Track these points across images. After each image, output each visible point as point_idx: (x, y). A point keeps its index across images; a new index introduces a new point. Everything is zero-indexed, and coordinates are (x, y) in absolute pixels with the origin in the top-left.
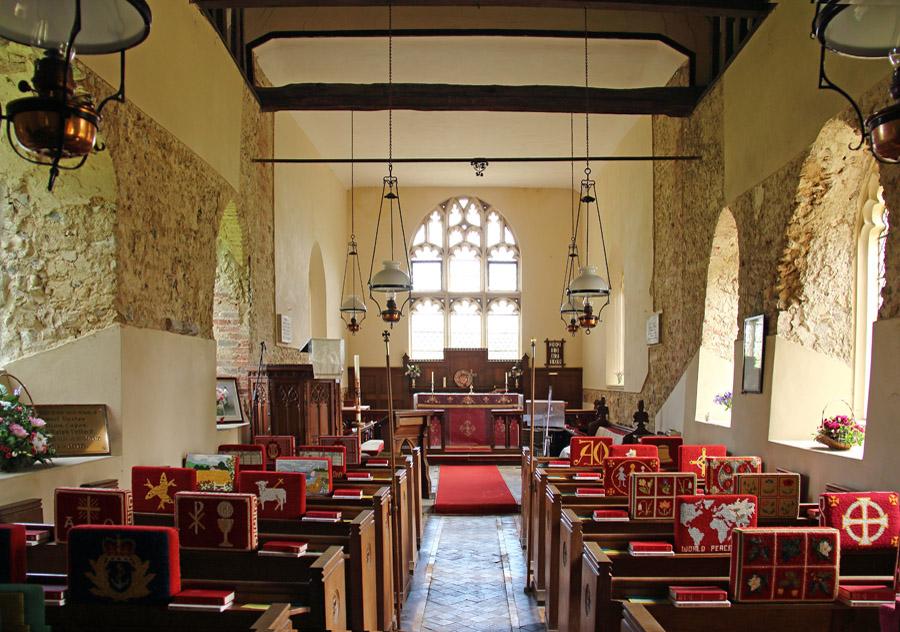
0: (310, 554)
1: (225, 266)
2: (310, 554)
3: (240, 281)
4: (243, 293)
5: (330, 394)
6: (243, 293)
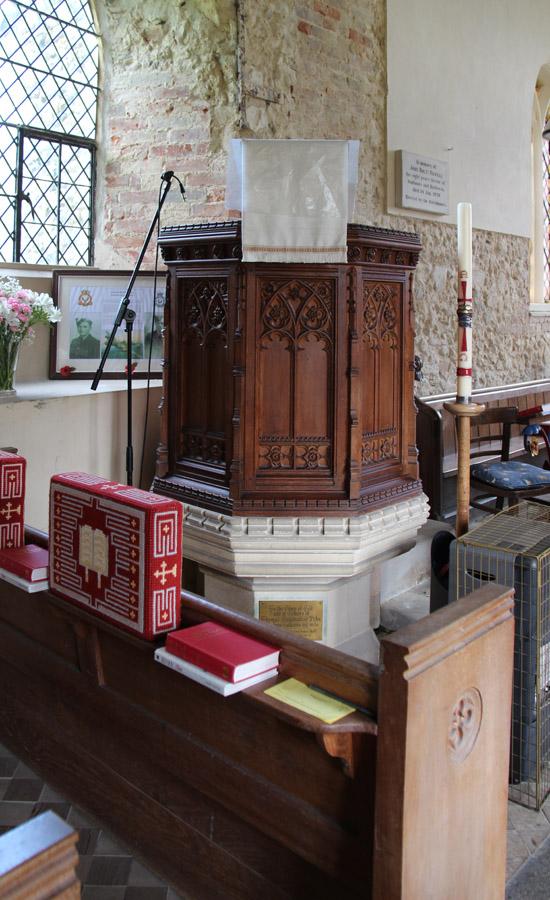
0: (87, 572)
1: (182, 30)
2: (87, 572)
3: (216, 59)
4: (223, 85)
5: (334, 308)
6: (223, 85)
